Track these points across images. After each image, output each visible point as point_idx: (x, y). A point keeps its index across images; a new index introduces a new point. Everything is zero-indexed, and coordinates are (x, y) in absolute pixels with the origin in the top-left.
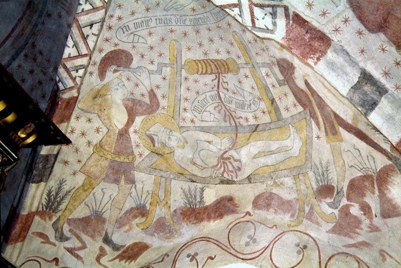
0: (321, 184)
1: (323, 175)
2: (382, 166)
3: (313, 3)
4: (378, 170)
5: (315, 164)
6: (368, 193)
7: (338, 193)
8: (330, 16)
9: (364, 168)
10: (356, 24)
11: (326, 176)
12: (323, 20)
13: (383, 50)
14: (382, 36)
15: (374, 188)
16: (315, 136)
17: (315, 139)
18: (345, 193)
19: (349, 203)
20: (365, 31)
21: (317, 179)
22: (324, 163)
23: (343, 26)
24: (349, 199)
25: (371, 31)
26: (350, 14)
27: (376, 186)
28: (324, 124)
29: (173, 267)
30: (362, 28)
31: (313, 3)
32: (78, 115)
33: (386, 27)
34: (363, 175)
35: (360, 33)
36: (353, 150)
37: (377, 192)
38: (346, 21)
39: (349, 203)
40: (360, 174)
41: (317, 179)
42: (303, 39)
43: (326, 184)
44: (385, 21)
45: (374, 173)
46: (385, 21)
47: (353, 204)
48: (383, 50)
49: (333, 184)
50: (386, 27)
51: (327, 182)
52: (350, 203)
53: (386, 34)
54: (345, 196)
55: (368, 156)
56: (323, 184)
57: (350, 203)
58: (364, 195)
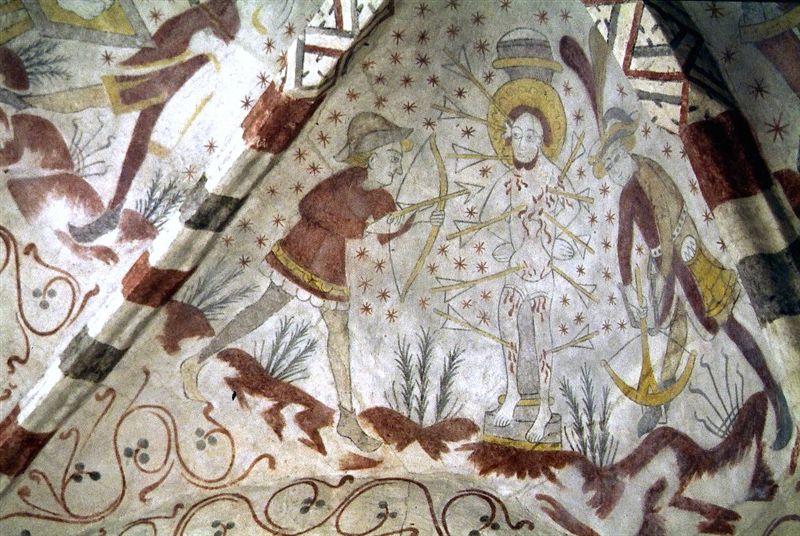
0: (23, 58)
1: (41, 63)
2: (95, 188)
3: (338, 123)
4: (87, 180)
5: (56, 45)
6: (39, 156)
7: (20, 97)
8: (320, 147)
9: (81, 151)
10: (310, 183)
11: (40, 68)
12: (314, 137)
13: (277, 221)
14: (296, 219)
15: (53, 168)
16: (110, 49)
17: (102, 49)
18: (24, 111)
19: (9, 119)
20: (301, 196)
21: (28, 50)
22: (63, 66)
23: (306, 164)
24: (17, 119)
25: (302, 204)
26: (324, 174)
27: (56, 171)
28: (136, 78)
29: (445, 534)
30: (306, 191)
31: (338, 123)
32: (245, 258)
33: (309, 225)
34: (387, 405)
35: (298, 188)
36: (105, 132)
37: (47, 173)
38: (314, 168)
39: (9, 119)
40: (68, 142)
41: (28, 50)
42: (288, 121)
43: (28, 70)
44: (317, 224)
45: (79, 170)
46: (317, 224)
47: (11, 127)
48: (277, 221)
49: (31, 86)
50: (309, 225)
51: (32, 73)
52: (10, 122)
53: (299, 224)
54: (20, 112)
55: (103, 162)
56: (26, 64)
57: (10, 122)
58: (33, 148)
